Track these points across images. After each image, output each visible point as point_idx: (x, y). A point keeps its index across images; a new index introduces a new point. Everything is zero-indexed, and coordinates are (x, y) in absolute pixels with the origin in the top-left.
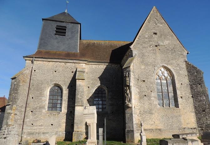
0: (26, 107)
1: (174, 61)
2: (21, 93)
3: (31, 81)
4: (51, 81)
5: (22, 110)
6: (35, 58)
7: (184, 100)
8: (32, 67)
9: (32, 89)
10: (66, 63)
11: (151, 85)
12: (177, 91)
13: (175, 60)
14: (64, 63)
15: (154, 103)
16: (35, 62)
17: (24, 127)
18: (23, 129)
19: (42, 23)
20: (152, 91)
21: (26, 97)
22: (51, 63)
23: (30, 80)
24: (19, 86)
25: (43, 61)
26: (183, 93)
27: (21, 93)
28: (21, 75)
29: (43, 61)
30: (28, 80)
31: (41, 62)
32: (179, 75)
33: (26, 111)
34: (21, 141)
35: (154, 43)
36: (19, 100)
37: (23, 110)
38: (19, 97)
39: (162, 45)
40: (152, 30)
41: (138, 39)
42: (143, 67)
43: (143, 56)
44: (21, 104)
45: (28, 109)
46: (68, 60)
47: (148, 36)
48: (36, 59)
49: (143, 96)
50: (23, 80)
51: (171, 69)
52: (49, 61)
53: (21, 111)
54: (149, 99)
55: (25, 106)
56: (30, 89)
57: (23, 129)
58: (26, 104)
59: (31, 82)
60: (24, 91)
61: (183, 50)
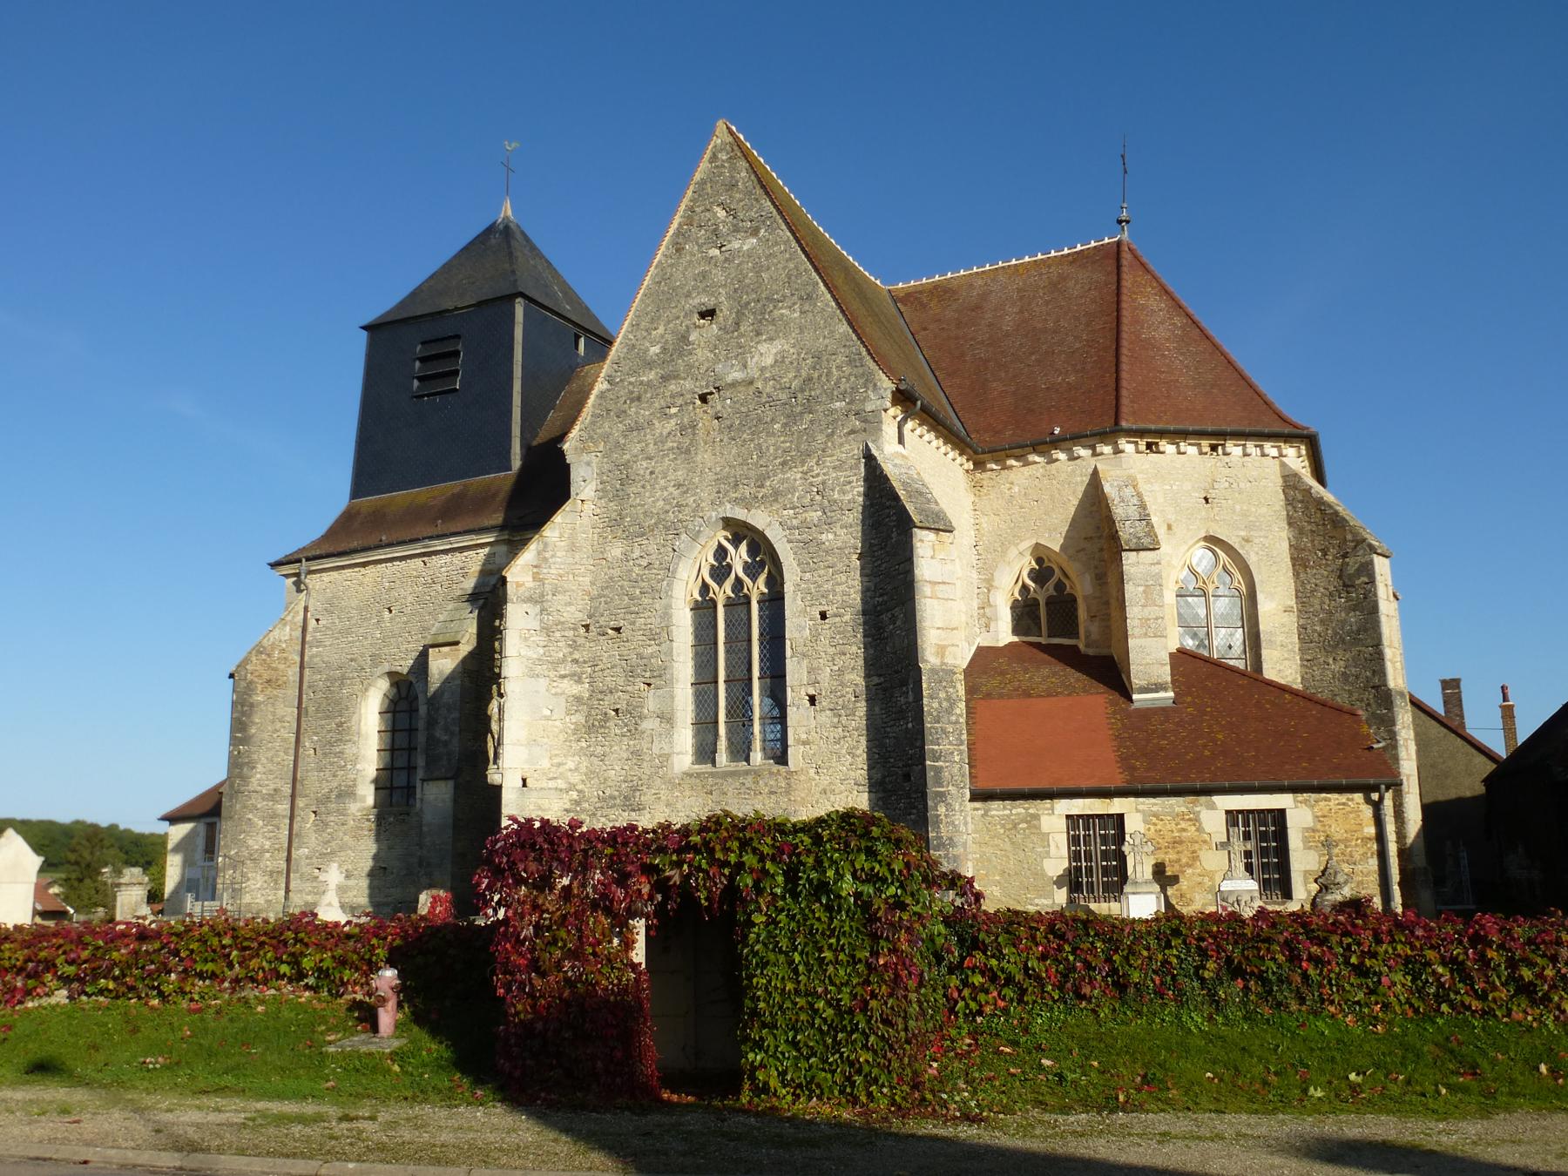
0: (293, 796)
1: (795, 475)
2: (266, 736)
3: (307, 672)
4: (376, 660)
5: (279, 812)
6: (308, 559)
7: (826, 718)
8: (306, 609)
9: (311, 709)
10: (425, 559)
11: (650, 650)
12: (788, 661)
13: (803, 463)
14: (418, 562)
15: (656, 750)
16: (312, 581)
17: (292, 885)
18: (287, 890)
19: (365, 334)
20: (649, 685)
21: (292, 752)
22: (370, 570)
23: (302, 667)
24: (252, 706)
25: (343, 567)
26: (825, 676)
27: (266, 736)
28: (254, 659)
29: (343, 567)
30: (293, 673)
31: (335, 574)
32: (808, 546)
33: (296, 813)
34: (1223, 1138)
35: (688, 384)
36: (260, 768)
37: (283, 808)
38: (255, 757)
39: (734, 384)
40: (688, 295)
41: (605, 386)
42: (616, 551)
43: (619, 484)
44: (272, 786)
45: (300, 803)
46: (427, 542)
47: (664, 350)
48: (315, 566)
49: (1173, 615)
50: (266, 676)
51: (768, 534)
52: (364, 565)
53: (274, 816)
54: (634, 732)
55: (290, 791)
56: (303, 711)
57: (287, 890)
58: (294, 779)
59: (306, 679)
60: (278, 725)
61: (870, 382)
